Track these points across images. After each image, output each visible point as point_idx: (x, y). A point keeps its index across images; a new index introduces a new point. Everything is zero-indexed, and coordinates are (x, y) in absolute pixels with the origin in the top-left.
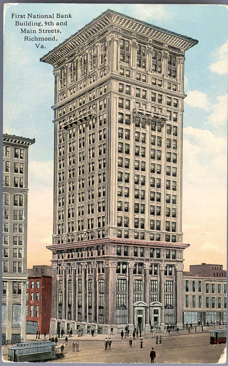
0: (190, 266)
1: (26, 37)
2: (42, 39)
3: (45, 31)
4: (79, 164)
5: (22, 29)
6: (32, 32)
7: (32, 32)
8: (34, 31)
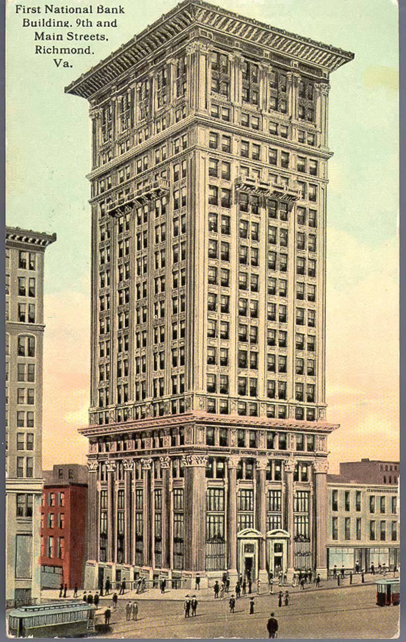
2: (67, 51)
8: (60, 37)
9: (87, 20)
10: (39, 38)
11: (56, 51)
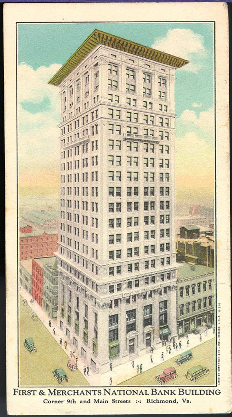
0: (127, 312)
1: (149, 400)
2: (163, 402)
3: (117, 402)
4: (89, 127)
5: (95, 400)
6: (105, 402)
7: (105, 402)
8: (107, 402)
9: (73, 400)
10: (97, 402)
11: (158, 402)
